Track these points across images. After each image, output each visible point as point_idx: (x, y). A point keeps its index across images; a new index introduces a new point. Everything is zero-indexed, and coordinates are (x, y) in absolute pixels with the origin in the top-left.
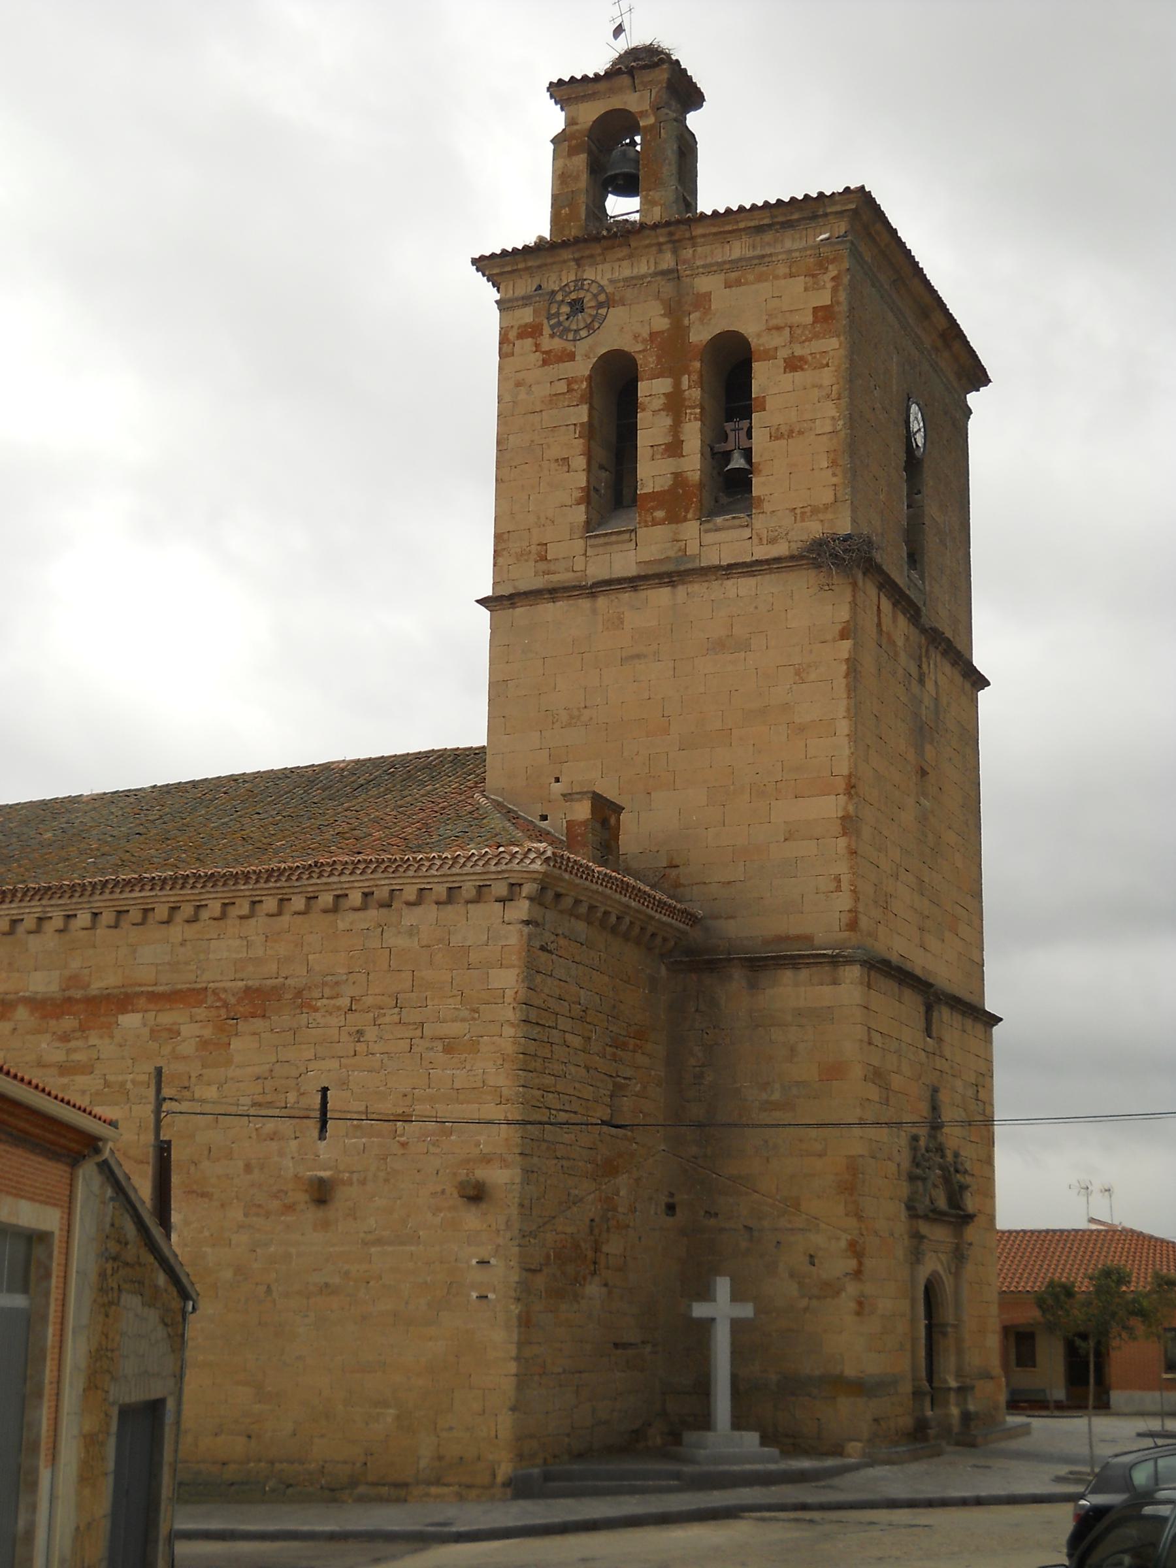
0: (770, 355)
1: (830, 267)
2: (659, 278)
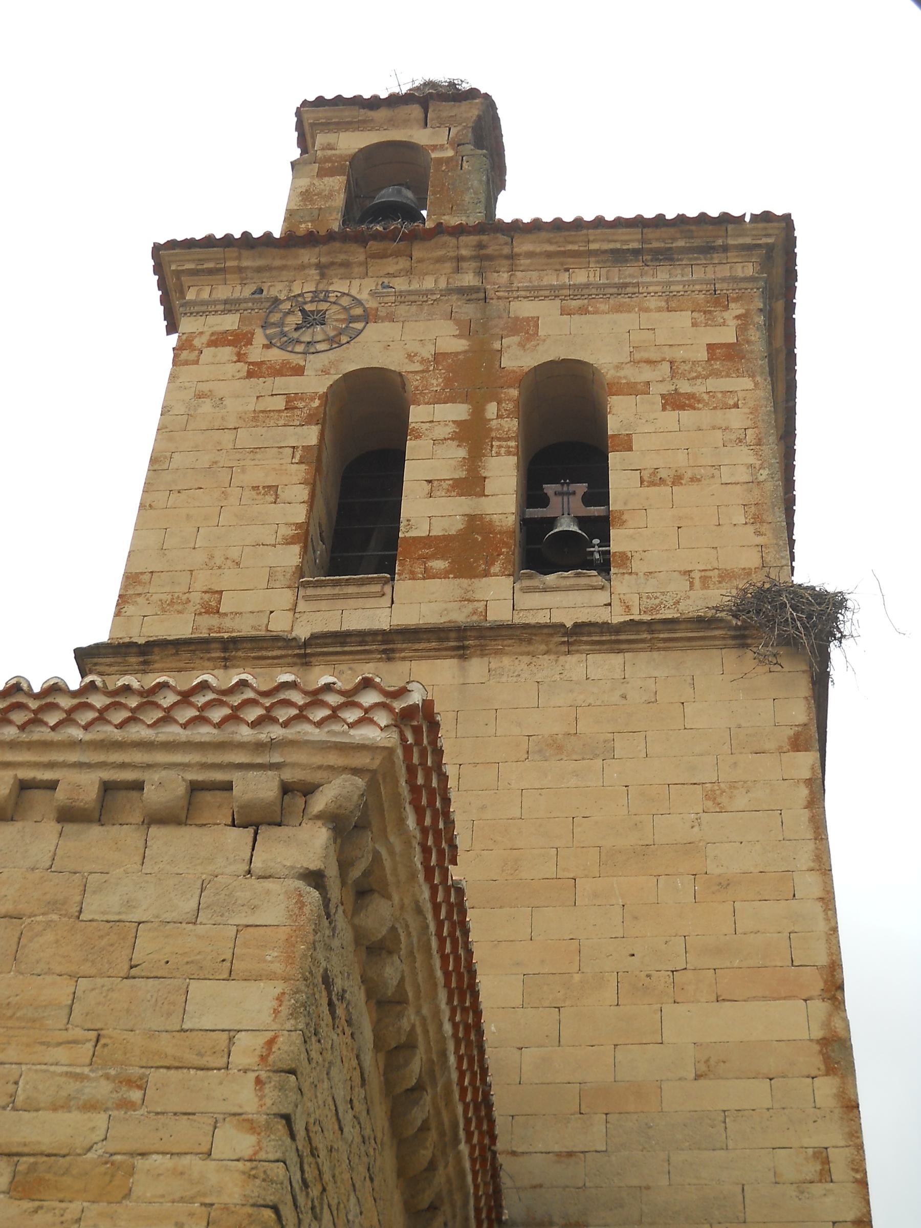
1: (732, 305)
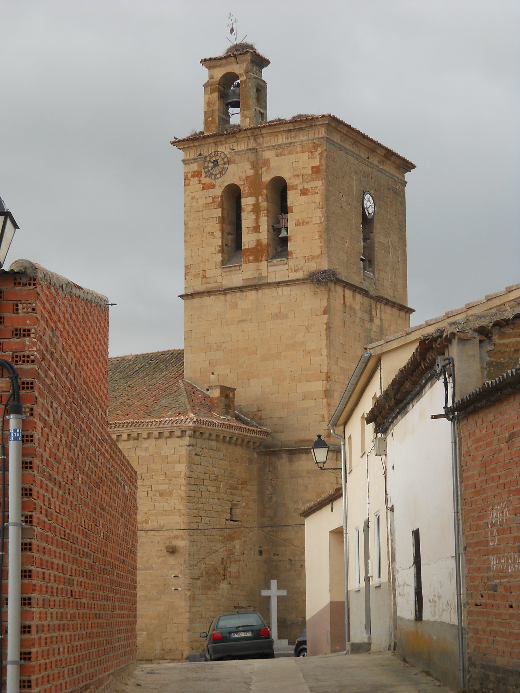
0: (294, 188)
1: (319, 149)
2: (249, 152)
